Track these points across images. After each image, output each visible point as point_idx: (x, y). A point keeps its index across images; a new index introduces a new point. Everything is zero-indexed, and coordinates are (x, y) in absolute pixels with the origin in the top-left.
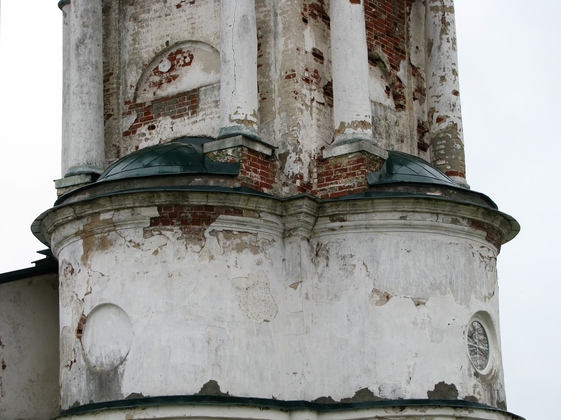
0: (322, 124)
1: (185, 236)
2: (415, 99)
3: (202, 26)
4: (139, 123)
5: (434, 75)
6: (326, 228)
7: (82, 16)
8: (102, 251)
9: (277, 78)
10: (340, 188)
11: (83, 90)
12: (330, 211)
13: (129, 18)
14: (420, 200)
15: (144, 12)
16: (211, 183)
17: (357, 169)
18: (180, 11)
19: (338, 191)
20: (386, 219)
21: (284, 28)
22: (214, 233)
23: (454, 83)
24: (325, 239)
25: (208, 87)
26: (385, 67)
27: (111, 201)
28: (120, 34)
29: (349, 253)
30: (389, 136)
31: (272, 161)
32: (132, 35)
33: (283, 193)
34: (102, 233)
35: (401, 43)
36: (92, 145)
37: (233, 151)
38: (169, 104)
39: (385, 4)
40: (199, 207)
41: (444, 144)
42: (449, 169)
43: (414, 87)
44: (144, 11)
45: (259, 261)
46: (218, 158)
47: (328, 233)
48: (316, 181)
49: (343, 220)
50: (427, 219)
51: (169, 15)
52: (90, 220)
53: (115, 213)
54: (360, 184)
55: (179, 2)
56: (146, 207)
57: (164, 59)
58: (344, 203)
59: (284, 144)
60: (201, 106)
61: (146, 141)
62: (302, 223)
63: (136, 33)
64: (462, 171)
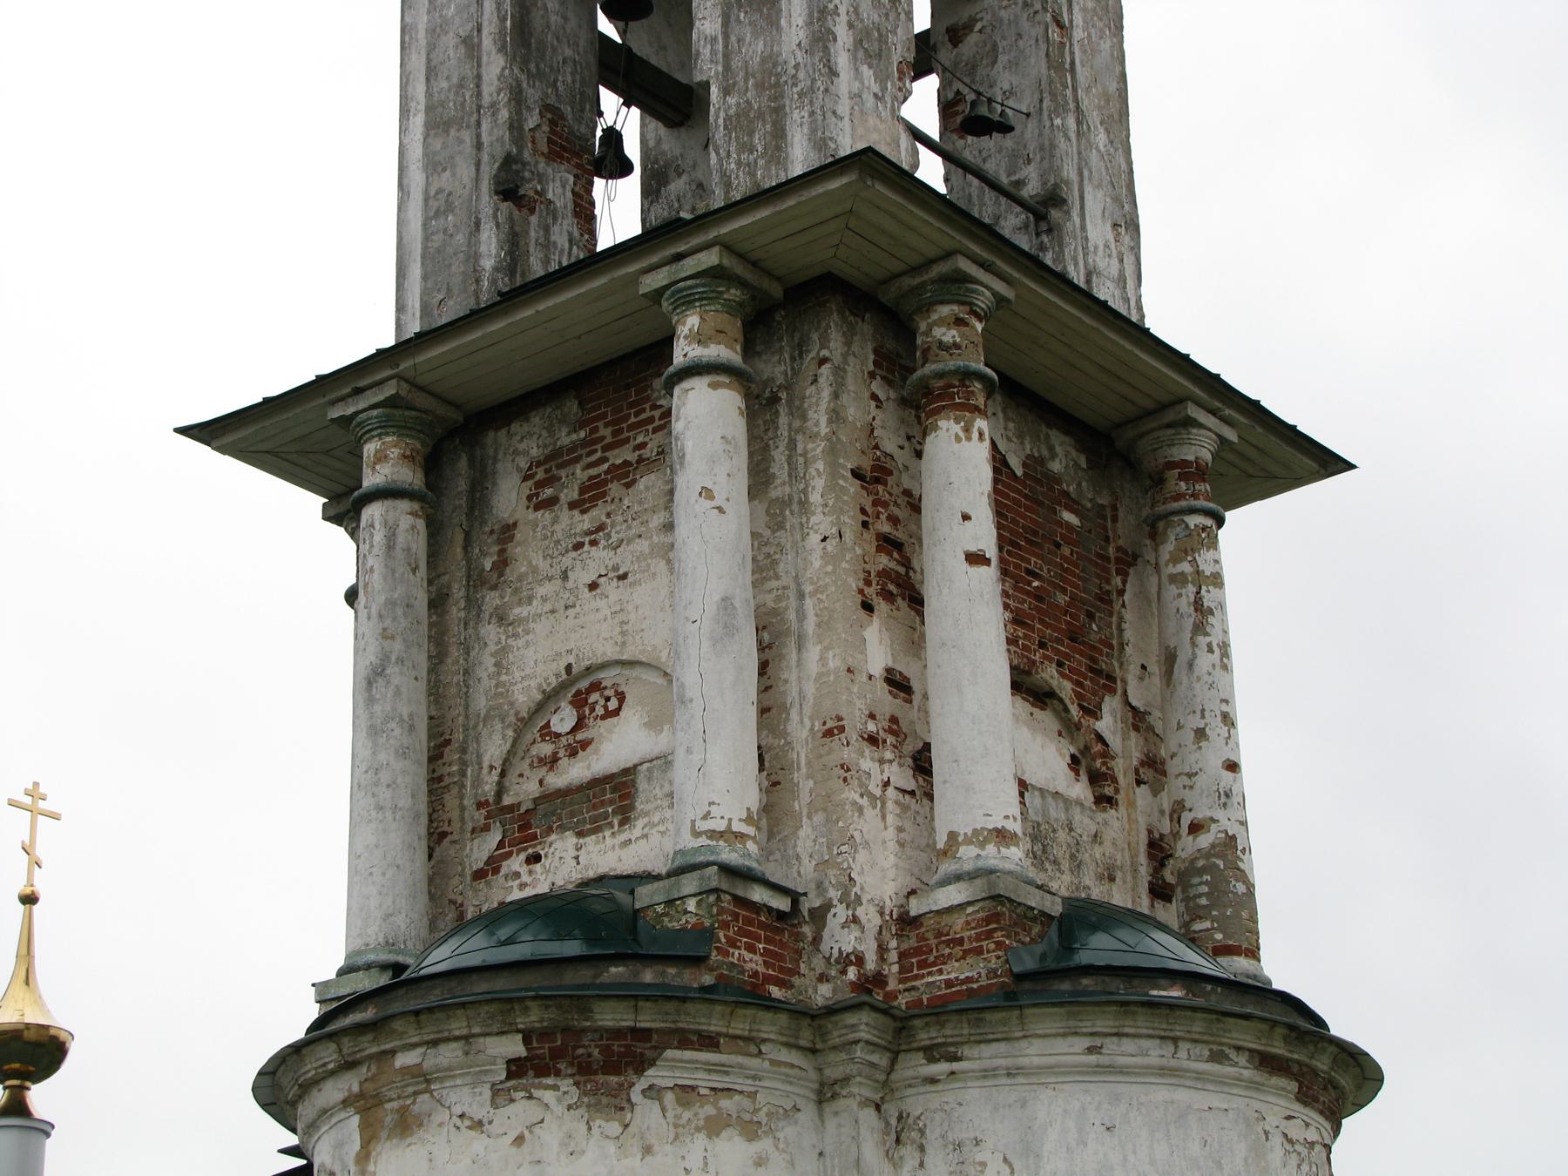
0: (909, 838)
1: (586, 1100)
2: (1139, 782)
3: (644, 626)
4: (507, 849)
5: (1179, 727)
6: (916, 1078)
7: (380, 616)
8: (401, 1139)
9: (804, 736)
10: (949, 984)
11: (379, 779)
12: (924, 1037)
13: (487, 617)
14: (1132, 1008)
15: (520, 603)
16: (648, 976)
17: (986, 939)
18: (595, 596)
19: (944, 992)
20: (1055, 1052)
21: (819, 625)
22: (652, 1092)
23: (1227, 743)
24: (916, 1103)
25: (655, 762)
26: (1066, 710)
27: (418, 1022)
28: (468, 653)
29: (972, 1135)
30: (1079, 866)
31: (794, 926)
32: (492, 655)
33: (819, 999)
34: (399, 1098)
35: (1104, 658)
36: (398, 901)
37: (699, 904)
38: (571, 804)
39: (1065, 570)
40: (617, 1033)
41: (1206, 883)
42: (1218, 941)
43: (1136, 756)
44: (520, 600)
45: (760, 1158)
46: (666, 919)
47: (922, 1089)
48: (895, 968)
49: (955, 1058)
50: (1151, 1052)
51: (574, 606)
52: (374, 1068)
53: (429, 1051)
54: (992, 973)
55: (594, 577)
56: (497, 1034)
57: (563, 704)
58: (954, 1017)
59: (820, 885)
60: (639, 806)
61: (521, 890)
62: (859, 1065)
63: (503, 648)
64: (1251, 945)
